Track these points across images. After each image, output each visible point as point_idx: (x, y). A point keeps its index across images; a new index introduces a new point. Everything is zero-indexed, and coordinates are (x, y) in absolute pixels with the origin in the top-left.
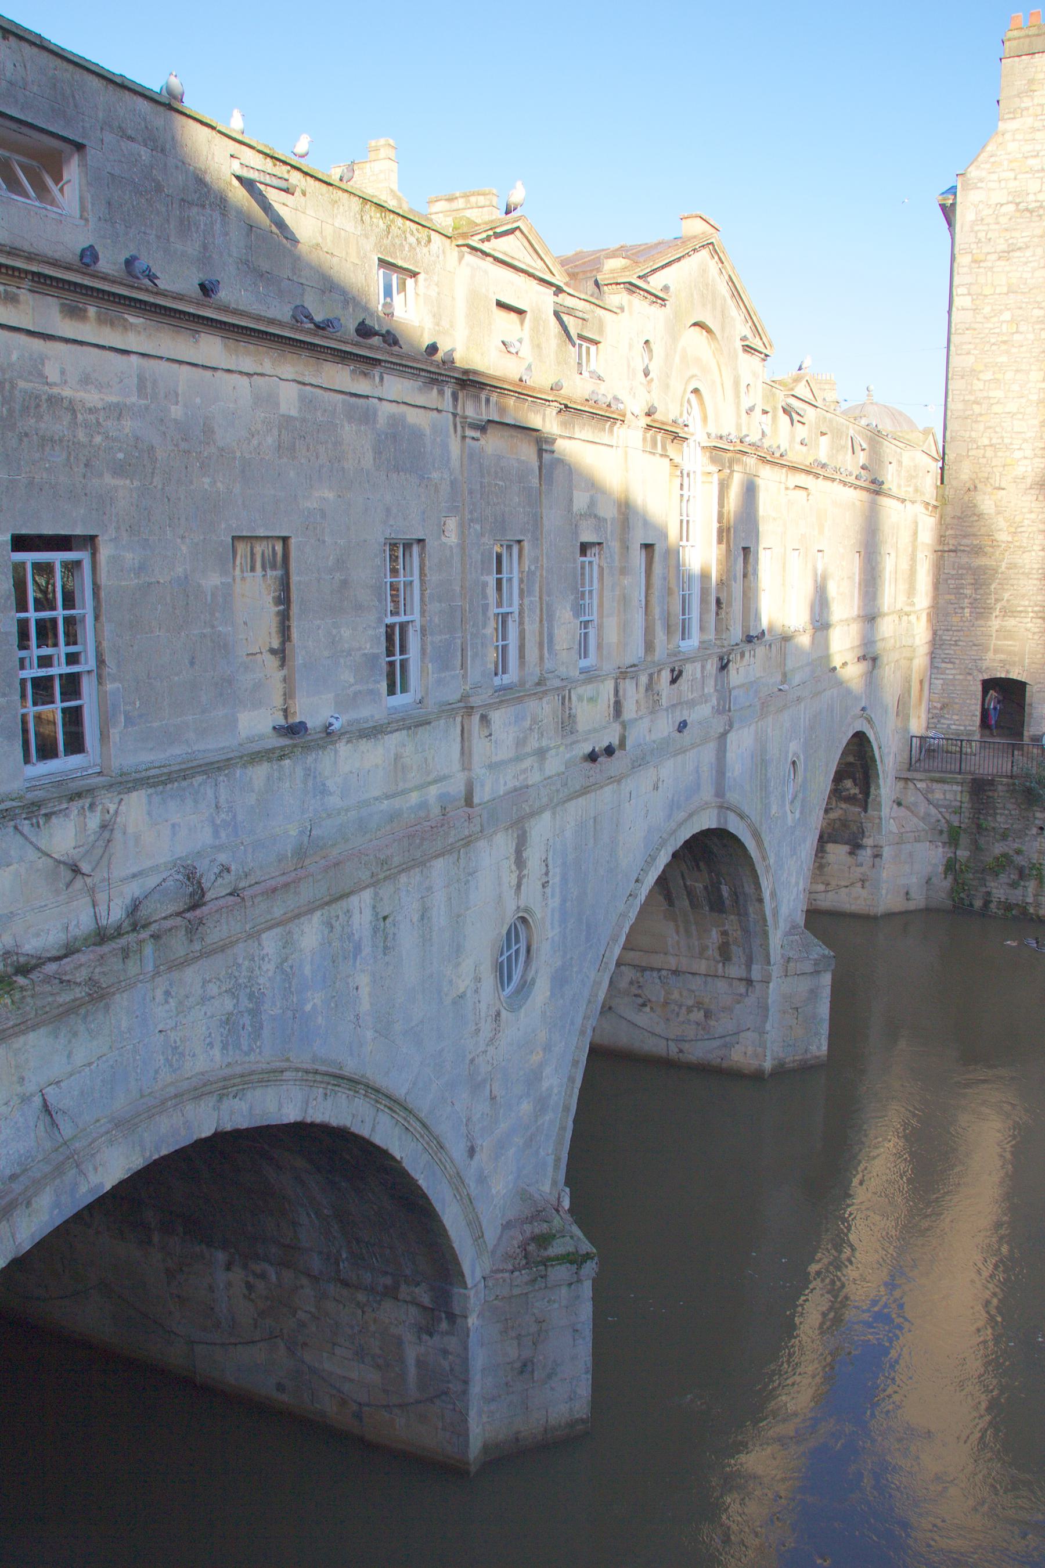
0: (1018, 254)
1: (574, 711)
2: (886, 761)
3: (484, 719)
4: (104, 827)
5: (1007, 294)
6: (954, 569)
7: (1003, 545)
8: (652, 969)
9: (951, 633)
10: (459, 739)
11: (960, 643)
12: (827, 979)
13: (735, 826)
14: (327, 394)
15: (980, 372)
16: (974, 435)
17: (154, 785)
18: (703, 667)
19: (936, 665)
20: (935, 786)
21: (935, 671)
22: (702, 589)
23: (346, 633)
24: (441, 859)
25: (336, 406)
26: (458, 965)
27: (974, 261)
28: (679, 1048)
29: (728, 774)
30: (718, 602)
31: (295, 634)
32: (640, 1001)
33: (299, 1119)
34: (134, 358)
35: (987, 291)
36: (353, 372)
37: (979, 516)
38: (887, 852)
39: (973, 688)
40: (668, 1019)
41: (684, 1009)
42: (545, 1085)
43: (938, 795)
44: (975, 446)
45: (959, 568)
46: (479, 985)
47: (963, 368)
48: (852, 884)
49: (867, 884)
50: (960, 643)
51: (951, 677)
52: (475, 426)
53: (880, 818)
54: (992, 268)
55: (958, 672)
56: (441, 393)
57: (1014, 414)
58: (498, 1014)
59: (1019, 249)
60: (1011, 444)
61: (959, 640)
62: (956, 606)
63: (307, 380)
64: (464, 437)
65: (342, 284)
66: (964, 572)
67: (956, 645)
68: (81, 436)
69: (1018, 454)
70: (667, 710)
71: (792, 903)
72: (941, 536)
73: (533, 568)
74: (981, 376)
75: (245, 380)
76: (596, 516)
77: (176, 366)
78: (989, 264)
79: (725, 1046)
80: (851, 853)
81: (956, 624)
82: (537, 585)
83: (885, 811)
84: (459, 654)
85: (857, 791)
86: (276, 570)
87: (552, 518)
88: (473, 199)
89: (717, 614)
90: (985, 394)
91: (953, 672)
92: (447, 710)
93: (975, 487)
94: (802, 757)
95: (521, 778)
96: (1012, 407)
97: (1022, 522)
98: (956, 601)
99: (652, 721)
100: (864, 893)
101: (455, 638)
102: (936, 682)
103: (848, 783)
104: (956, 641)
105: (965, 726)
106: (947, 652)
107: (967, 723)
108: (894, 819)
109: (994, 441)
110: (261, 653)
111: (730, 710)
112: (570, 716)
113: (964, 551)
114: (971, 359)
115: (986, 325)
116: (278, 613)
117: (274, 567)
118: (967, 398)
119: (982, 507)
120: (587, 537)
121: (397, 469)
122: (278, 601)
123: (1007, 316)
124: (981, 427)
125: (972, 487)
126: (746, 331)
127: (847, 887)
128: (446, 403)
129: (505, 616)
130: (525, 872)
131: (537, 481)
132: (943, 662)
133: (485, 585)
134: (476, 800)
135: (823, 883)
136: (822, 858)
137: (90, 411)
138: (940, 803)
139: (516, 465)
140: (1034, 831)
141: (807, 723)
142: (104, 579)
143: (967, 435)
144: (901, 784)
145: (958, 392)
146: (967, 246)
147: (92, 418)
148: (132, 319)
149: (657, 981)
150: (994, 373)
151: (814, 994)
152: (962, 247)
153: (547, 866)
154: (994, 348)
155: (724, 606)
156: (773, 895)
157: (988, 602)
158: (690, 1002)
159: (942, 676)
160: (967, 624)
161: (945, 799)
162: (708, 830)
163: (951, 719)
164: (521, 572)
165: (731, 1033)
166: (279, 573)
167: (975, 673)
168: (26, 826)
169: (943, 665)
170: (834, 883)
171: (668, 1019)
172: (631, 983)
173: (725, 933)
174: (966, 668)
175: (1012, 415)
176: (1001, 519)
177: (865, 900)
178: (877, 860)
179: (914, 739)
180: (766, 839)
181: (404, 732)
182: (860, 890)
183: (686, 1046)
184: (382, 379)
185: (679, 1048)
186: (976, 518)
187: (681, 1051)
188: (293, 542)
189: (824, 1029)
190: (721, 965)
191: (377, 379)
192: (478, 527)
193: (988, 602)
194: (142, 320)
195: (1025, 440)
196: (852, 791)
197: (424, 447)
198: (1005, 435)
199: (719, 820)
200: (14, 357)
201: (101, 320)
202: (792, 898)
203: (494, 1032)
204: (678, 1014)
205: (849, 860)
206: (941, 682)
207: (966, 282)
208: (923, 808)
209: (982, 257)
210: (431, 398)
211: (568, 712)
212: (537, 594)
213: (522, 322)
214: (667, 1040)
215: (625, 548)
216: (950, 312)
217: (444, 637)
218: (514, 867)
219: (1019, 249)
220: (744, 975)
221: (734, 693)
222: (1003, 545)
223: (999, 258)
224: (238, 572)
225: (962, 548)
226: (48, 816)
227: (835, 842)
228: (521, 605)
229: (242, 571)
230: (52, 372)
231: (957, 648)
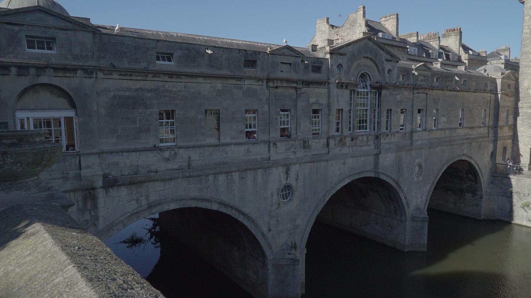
3: (275, 144)
4: (175, 153)
11: (523, 136)
13: (383, 177)
14: (229, 85)
16: (529, 72)
17: (184, 148)
18: (367, 138)
24: (260, 170)
30: (378, 122)
31: (221, 126)
33: (217, 210)
34: (183, 83)
42: (297, 223)
44: (529, 75)
46: (335, 143)
47: (526, 51)
52: (271, 87)
56: (263, 82)
58: (279, 204)
61: (523, 135)
62: (522, 125)
63: (224, 83)
64: (269, 90)
66: (525, 114)
67: (522, 137)
68: (172, 95)
70: (349, 147)
75: (209, 84)
76: (318, 103)
77: (192, 83)
80: (473, 196)
81: (521, 130)
85: (473, 178)
88: (391, 17)
89: (378, 125)
92: (264, 142)
93: (529, 88)
94: (423, 164)
98: (522, 123)
103: (470, 175)
104: (522, 136)
108: (489, 187)
114: (529, 48)
117: (216, 114)
118: (527, 60)
120: (316, 107)
122: (217, 120)
125: (528, 88)
126: (389, 57)
127: (471, 206)
128: (264, 84)
129: (340, 111)
134: (271, 159)
135: (464, 204)
137: (174, 91)
142: (176, 116)
143: (527, 72)
145: (524, 59)
146: (528, 14)
147: (175, 93)
148: (182, 77)
152: (526, 14)
153: (298, 176)
155: (379, 123)
159: (516, 146)
160: (525, 130)
166: (218, 116)
167: (528, 146)
168: (159, 152)
173: (395, 207)
174: (525, 144)
181: (251, 145)
184: (244, 81)
187: (385, 237)
188: (220, 110)
189: (426, 237)
190: (395, 215)
191: (243, 81)
192: (274, 107)
194: (184, 77)
196: (472, 178)
200: (160, 85)
201: (176, 78)
206: (516, 148)
207: (527, 25)
210: (260, 83)
212: (296, 119)
215: (330, 110)
218: (285, 174)
221: (382, 145)
224: (208, 115)
225: (524, 107)
226: (164, 151)
229: (209, 115)
230: (167, 86)
231: (522, 138)
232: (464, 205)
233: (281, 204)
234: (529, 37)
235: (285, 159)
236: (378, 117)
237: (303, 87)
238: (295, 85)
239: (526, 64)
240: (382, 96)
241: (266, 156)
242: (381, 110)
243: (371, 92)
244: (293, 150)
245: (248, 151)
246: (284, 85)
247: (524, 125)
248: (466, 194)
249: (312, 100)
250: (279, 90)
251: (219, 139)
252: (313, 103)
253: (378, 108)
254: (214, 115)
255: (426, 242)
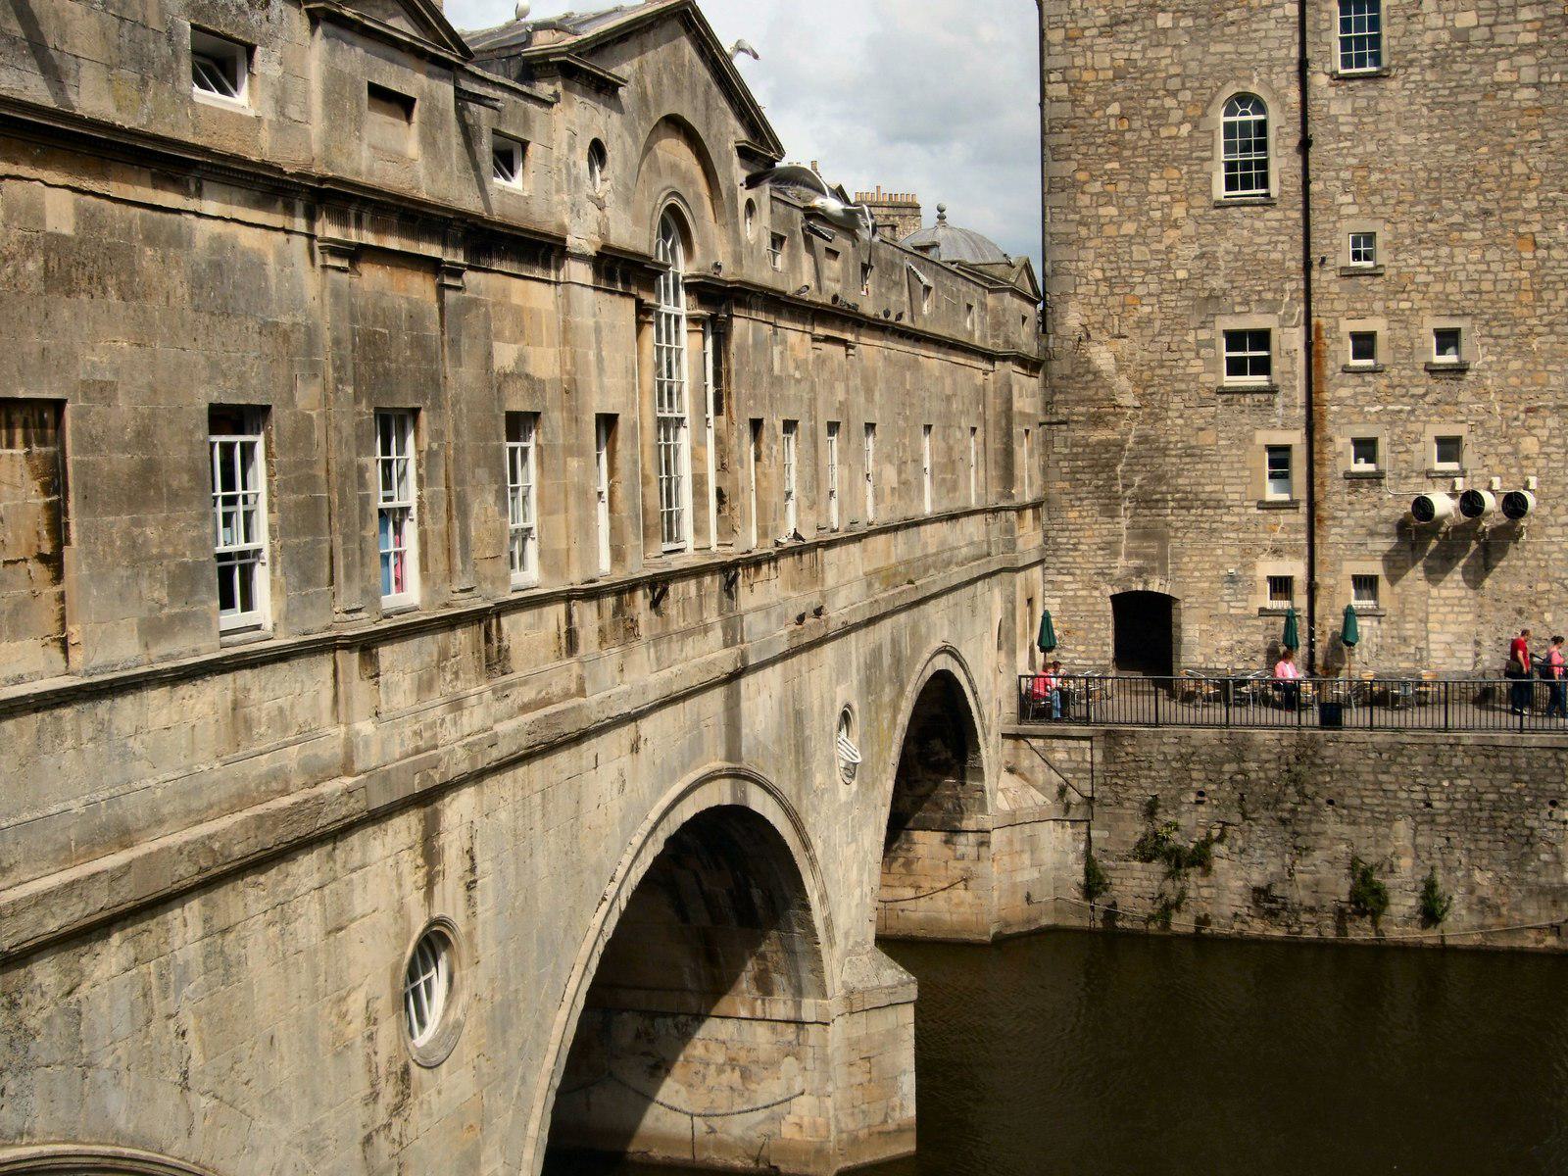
0: (1124, 28)
1: (505, 643)
2: (986, 710)
5: (1113, 80)
6: (1066, 446)
7: (1130, 412)
8: (664, 1015)
9: (1067, 534)
10: (330, 683)
12: (908, 1014)
13: (758, 802)
15: (1085, 183)
19: (1050, 578)
20: (1056, 743)
21: (1050, 586)
22: (694, 476)
23: (151, 532)
25: (131, 222)
26: (342, 1000)
27: (1068, 38)
28: (710, 1127)
29: (745, 731)
32: (651, 1061)
35: (1087, 76)
36: (153, 175)
37: (1095, 374)
38: (996, 837)
39: (1099, 607)
40: (691, 1085)
41: (713, 1068)
43: (1061, 755)
45: (1074, 445)
46: (374, 1028)
48: (951, 886)
49: (971, 884)
50: (1081, 547)
51: (1071, 593)
53: (982, 790)
54: (1092, 46)
55: (1080, 586)
57: (1132, 237)
59: (1125, 22)
60: (1131, 276)
64: (325, 267)
65: (383, 104)
66: (1080, 450)
67: (1076, 550)
69: (1140, 290)
71: (853, 911)
72: (1047, 403)
73: (435, 446)
74: (1087, 188)
76: (527, 376)
78: (1088, 41)
79: (772, 1119)
80: (946, 842)
82: (442, 471)
83: (989, 781)
84: (327, 563)
85: (950, 754)
86: (46, 445)
87: (462, 377)
89: (719, 511)
90: (1093, 212)
91: (1074, 586)
93: (1088, 336)
95: (427, 735)
96: (1129, 228)
97: (1152, 380)
99: (624, 657)
100: (968, 896)
101: (320, 542)
102: (1051, 601)
103: (936, 744)
105: (1093, 659)
106: (1064, 559)
107: (1096, 655)
109: (1108, 274)
110: (25, 560)
111: (742, 642)
112: (499, 651)
113: (1077, 422)
114: (1074, 165)
115: (1089, 121)
116: (49, 506)
118: (1071, 217)
119: (1098, 362)
120: (518, 404)
121: (226, 313)
122: (46, 490)
123: (1115, 109)
124: (1091, 255)
127: (944, 889)
130: (439, 868)
131: (438, 327)
132: (1060, 573)
133: (362, 471)
134: (358, 766)
135: (911, 886)
136: (909, 850)
138: (1065, 765)
139: (405, 305)
140: (1193, 797)
141: (862, 660)
143: (1073, 266)
144: (1009, 743)
149: (674, 1032)
150: (1103, 184)
151: (893, 1036)
152: (1052, 19)
154: (1101, 150)
156: (824, 898)
157: (1114, 489)
158: (720, 1058)
161: (1070, 760)
162: (718, 807)
163: (1076, 651)
164: (419, 452)
165: (779, 1099)
169: (1060, 578)
170: (926, 885)
171: (691, 1085)
172: (638, 1036)
175: (1130, 239)
176: (1123, 377)
177: (971, 906)
178: (983, 849)
179: (1024, 680)
180: (810, 821)
181: (247, 673)
182: (962, 892)
183: (716, 1122)
185: (710, 1127)
186: (1090, 377)
187: (712, 1131)
192: (350, 390)
193: (1114, 489)
195: (1147, 271)
197: (266, 281)
198: (1121, 264)
199: (734, 794)
202: (854, 904)
203: (400, 1097)
204: (704, 1077)
205: (947, 852)
206: (1058, 600)
208: (1041, 774)
209: (1076, 33)
211: (496, 644)
212: (443, 481)
213: (408, 117)
214: (692, 1116)
216: (1042, 105)
217: (303, 539)
218: (420, 861)
219: (1125, 22)
220: (792, 1015)
222: (1130, 412)
223: (1101, 34)
227: (925, 829)
228: (419, 497)
232: (909, 893)
233: (415, 1070)
234: (1070, 119)
235: (417, 751)
236: (722, 468)
237: (471, 268)
238: (433, 251)
239: (1068, 234)
240: (733, 348)
241: (331, 742)
242: (731, 422)
243: (692, 320)
244: (444, 686)
245: (239, 719)
246: (393, 243)
247: (1080, 499)
248: (918, 835)
249: (505, 356)
250: (373, 276)
251: (64, 646)
252: (506, 375)
253: (718, 411)
254: (27, 443)
255: (911, 1111)
